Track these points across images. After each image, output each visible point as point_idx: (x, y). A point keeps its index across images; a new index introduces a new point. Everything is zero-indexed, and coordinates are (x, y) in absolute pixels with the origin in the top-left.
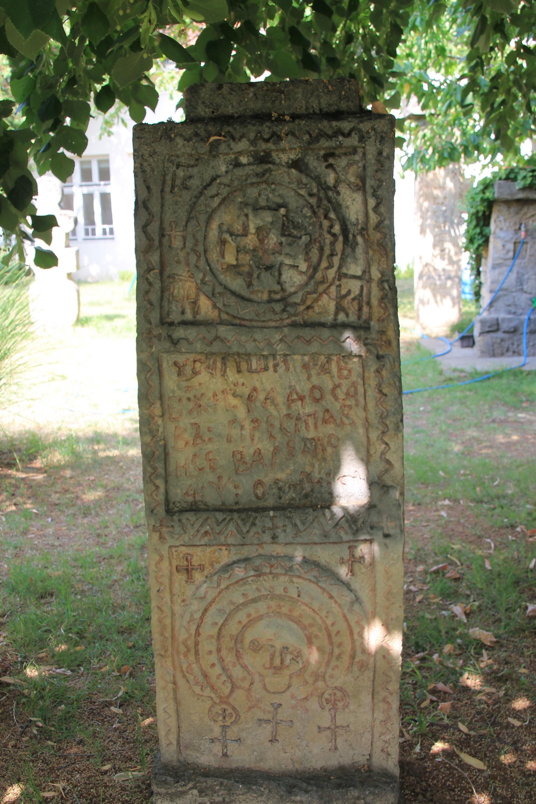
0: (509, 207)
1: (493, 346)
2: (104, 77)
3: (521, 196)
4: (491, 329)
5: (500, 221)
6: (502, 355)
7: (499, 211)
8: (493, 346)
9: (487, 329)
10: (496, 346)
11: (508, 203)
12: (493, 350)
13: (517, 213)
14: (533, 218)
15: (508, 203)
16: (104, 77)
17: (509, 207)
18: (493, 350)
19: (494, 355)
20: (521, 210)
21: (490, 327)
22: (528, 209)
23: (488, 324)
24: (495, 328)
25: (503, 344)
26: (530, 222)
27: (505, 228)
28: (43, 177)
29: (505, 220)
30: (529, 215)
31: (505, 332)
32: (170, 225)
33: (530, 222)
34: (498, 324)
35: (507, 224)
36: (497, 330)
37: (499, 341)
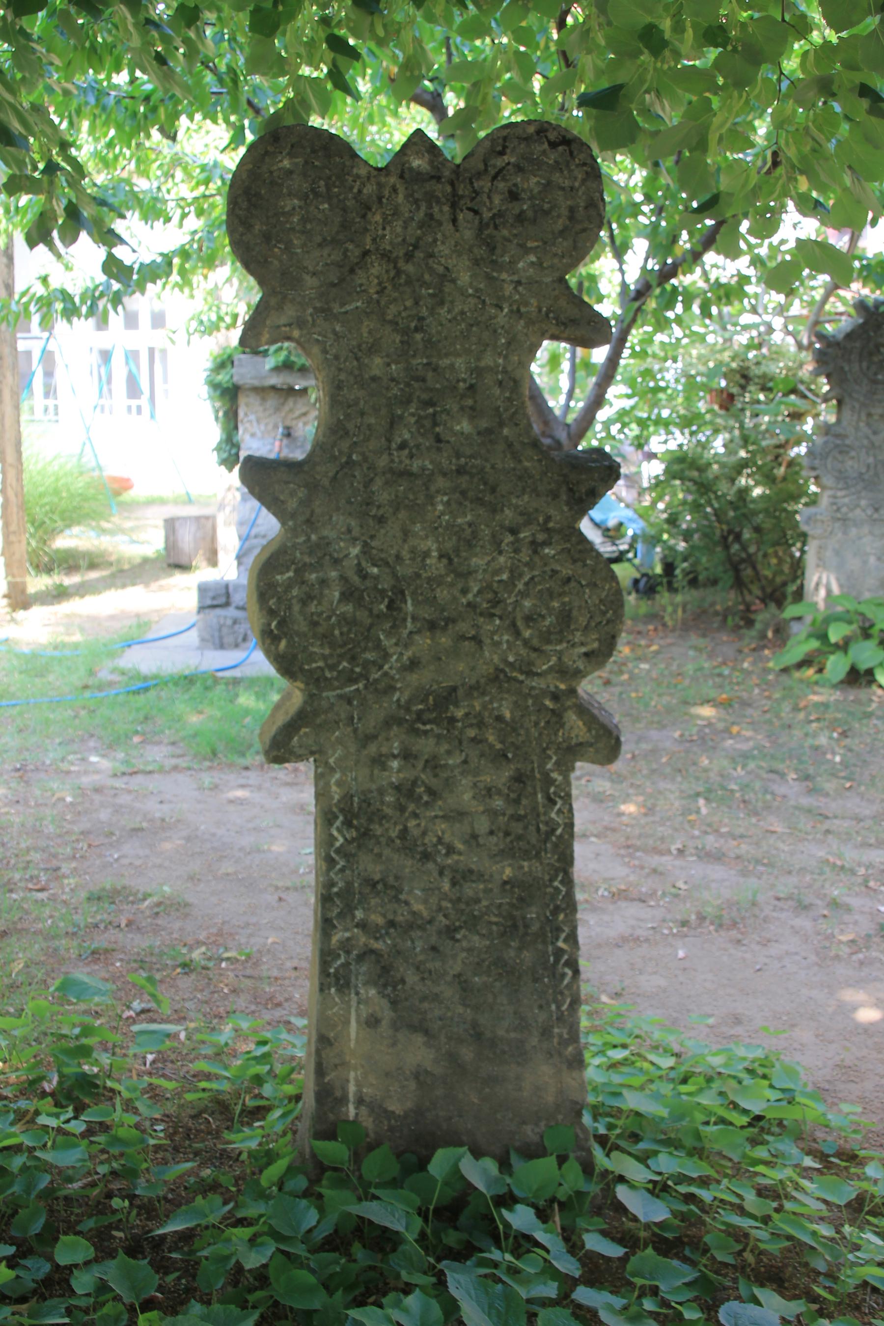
0: (264, 399)
1: (220, 630)
2: (322, 65)
3: (275, 380)
4: (215, 603)
5: (250, 422)
6: (237, 646)
7: (247, 405)
8: (220, 630)
9: (209, 602)
10: (225, 630)
11: (262, 391)
12: (221, 638)
13: (277, 410)
14: (304, 419)
15: (262, 391)
16: (322, 65)
17: (264, 399)
18: (221, 638)
19: (222, 646)
20: (283, 404)
21: (214, 598)
22: (295, 403)
23: (211, 594)
24: (222, 600)
25: (237, 627)
26: (301, 425)
27: (259, 434)
28: (73, 248)
29: (258, 421)
30: (297, 413)
31: (238, 608)
32: (234, 324)
33: (301, 425)
34: (228, 595)
35: (262, 428)
36: (227, 604)
37: (229, 622)
